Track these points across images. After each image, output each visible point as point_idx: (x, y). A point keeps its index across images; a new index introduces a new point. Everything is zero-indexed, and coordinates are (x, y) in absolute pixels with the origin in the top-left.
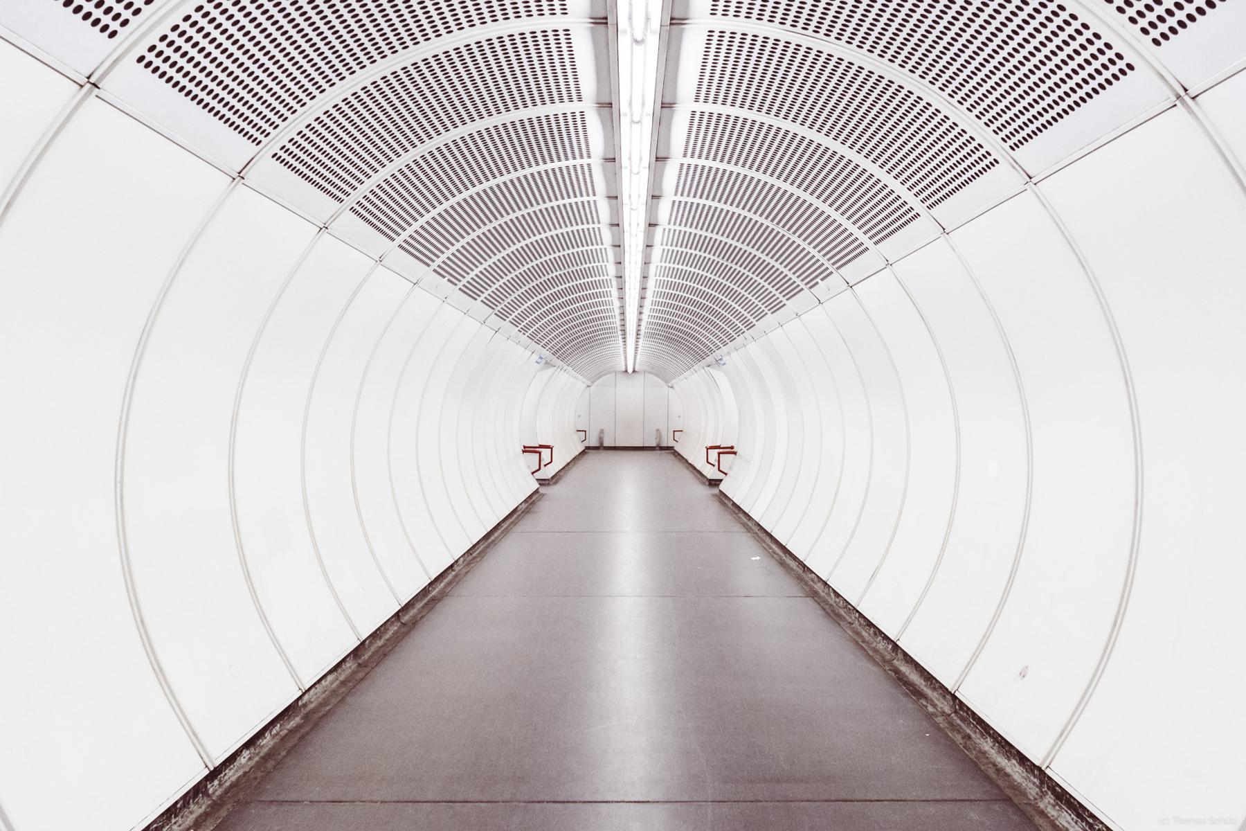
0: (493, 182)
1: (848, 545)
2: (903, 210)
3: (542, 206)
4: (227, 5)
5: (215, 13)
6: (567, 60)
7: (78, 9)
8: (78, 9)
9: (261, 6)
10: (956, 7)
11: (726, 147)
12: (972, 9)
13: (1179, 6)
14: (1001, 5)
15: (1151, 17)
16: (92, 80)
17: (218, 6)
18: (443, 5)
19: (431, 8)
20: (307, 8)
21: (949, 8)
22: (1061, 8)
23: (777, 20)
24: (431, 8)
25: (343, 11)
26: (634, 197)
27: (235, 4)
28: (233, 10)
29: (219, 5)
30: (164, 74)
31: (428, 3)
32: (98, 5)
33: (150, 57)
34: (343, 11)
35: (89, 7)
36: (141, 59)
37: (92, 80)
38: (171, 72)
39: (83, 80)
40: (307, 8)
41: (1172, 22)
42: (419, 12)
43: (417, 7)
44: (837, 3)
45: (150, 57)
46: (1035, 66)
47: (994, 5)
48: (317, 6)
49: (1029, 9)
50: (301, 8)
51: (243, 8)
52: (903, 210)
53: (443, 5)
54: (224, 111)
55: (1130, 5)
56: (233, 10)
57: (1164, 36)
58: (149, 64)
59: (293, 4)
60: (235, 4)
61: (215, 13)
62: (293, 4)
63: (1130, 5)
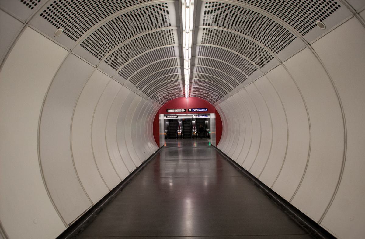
0: (169, 80)
1: (19, 21)
2: (240, 74)
3: (168, 86)
4: (70, 1)
5: (66, 4)
6: (167, 20)
7: (25, 3)
8: (25, 3)
9: (79, 1)
10: (272, 2)
11: (207, 53)
12: (281, 3)
13: (305, 2)
14: (289, 1)
15: (331, 4)
16: (95, 67)
17: (67, 2)
18: (131, 1)
19: (128, 3)
20: (87, 2)
21: (274, 3)
22: (336, 3)
23: (260, 7)
24: (128, 3)
25: (78, 4)
26: (187, 79)
27: (72, 1)
28: (71, 3)
29: (68, 1)
30: (50, 21)
31: (127, 1)
32: (60, 1)
33: (44, 14)
34: (78, 4)
35: (28, 2)
36: (41, 15)
37: (95, 67)
38: (54, 22)
39: (69, 50)
40: (87, 2)
41: (334, 7)
42: (120, 4)
43: (120, 2)
44: (255, 1)
45: (44, 14)
46: (309, 24)
47: (291, 2)
48: (90, 2)
49: (301, 3)
50: (86, 2)
51: (74, 2)
52: (240, 74)
53: (131, 1)
54: (86, 47)
55: (301, 1)
56: (71, 3)
57: (332, 11)
58: (48, 19)
59: (103, 1)
60: (72, 1)
61: (66, 4)
62: (103, 1)
63: (301, 1)
